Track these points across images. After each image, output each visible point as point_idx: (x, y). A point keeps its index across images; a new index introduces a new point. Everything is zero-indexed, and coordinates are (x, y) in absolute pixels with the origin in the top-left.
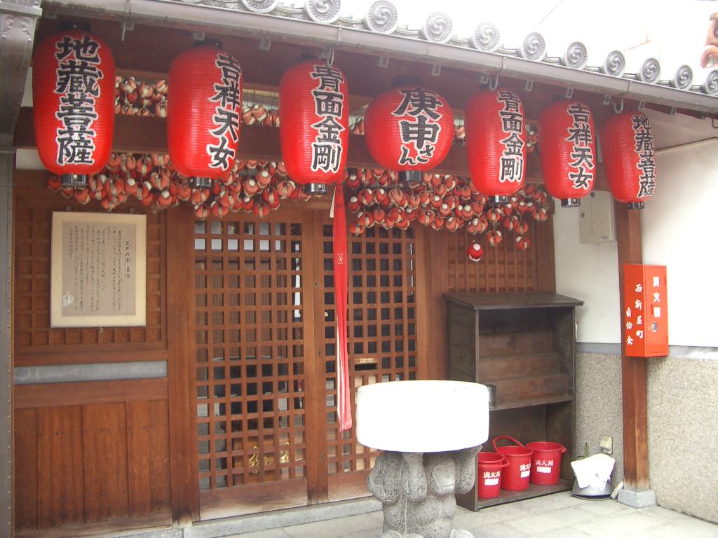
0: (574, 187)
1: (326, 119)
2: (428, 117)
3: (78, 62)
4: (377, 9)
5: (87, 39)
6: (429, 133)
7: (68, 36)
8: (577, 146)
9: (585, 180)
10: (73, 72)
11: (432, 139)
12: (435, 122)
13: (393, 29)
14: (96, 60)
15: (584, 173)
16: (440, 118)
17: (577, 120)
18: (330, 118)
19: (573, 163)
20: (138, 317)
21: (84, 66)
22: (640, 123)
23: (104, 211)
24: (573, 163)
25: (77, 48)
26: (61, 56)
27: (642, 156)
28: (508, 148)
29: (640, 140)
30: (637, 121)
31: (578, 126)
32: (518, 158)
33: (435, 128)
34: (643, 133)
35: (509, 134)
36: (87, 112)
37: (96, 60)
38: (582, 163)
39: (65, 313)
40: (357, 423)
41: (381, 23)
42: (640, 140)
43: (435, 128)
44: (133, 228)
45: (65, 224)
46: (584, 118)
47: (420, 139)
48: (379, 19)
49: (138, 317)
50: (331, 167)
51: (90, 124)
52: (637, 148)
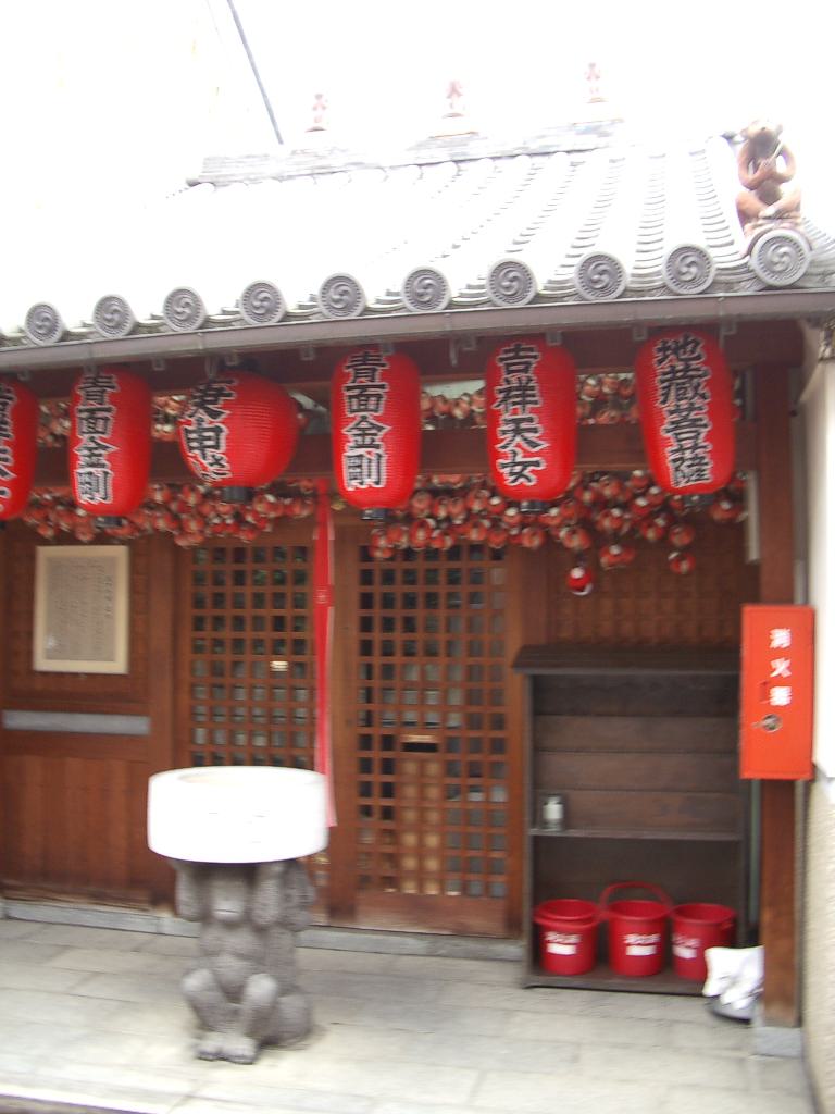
0: (506, 483)
1: (358, 419)
2: (207, 418)
3: (680, 366)
4: (416, 282)
5: (686, 337)
6: (209, 438)
7: (666, 339)
8: (507, 416)
9: (523, 470)
10: (674, 378)
11: (216, 447)
12: (217, 422)
13: (444, 303)
14: (698, 358)
15: (519, 459)
16: (223, 416)
17: (509, 372)
18: (364, 419)
19: (502, 444)
20: (118, 664)
21: (687, 369)
22: (669, 352)
23: (77, 542)
24: (502, 444)
25: (675, 352)
26: (660, 362)
27: (672, 413)
28: (352, 439)
29: (666, 384)
30: (664, 349)
31: (508, 381)
32: (369, 453)
33: (218, 430)
34: (673, 371)
35: (354, 418)
36: (699, 423)
37: (698, 358)
38: (514, 443)
39: (50, 656)
40: (709, 974)
41: (427, 299)
42: (666, 384)
43: (218, 430)
44: (112, 561)
45: (50, 560)
46: (521, 367)
47: (214, 447)
48: (421, 295)
49: (118, 664)
50: (707, 474)
51: (702, 436)
52: (662, 398)
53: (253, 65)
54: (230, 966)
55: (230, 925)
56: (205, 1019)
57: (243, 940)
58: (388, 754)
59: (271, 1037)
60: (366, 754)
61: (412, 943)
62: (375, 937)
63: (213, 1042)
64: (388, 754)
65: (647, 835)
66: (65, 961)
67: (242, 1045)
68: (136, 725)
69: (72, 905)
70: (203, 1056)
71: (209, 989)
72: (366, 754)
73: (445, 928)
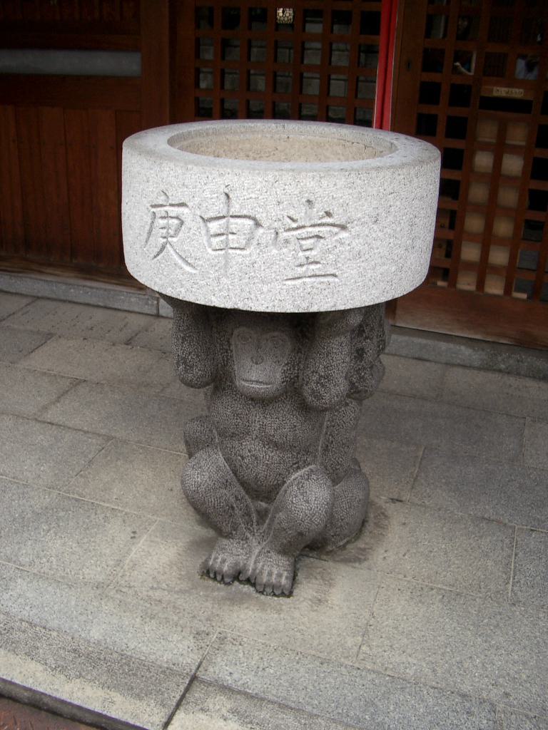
53: (142, 314)
54: (258, 457)
55: (262, 402)
56: (213, 519)
57: (283, 422)
58: (459, 111)
59: (313, 547)
60: (428, 109)
61: (465, 352)
62: (423, 341)
63: (227, 557)
64: (459, 111)
65: (492, 112)
66: (41, 360)
67: (274, 568)
68: (125, 64)
69: (59, 279)
70: (209, 573)
71: (226, 484)
72: (428, 109)
73: (505, 336)
